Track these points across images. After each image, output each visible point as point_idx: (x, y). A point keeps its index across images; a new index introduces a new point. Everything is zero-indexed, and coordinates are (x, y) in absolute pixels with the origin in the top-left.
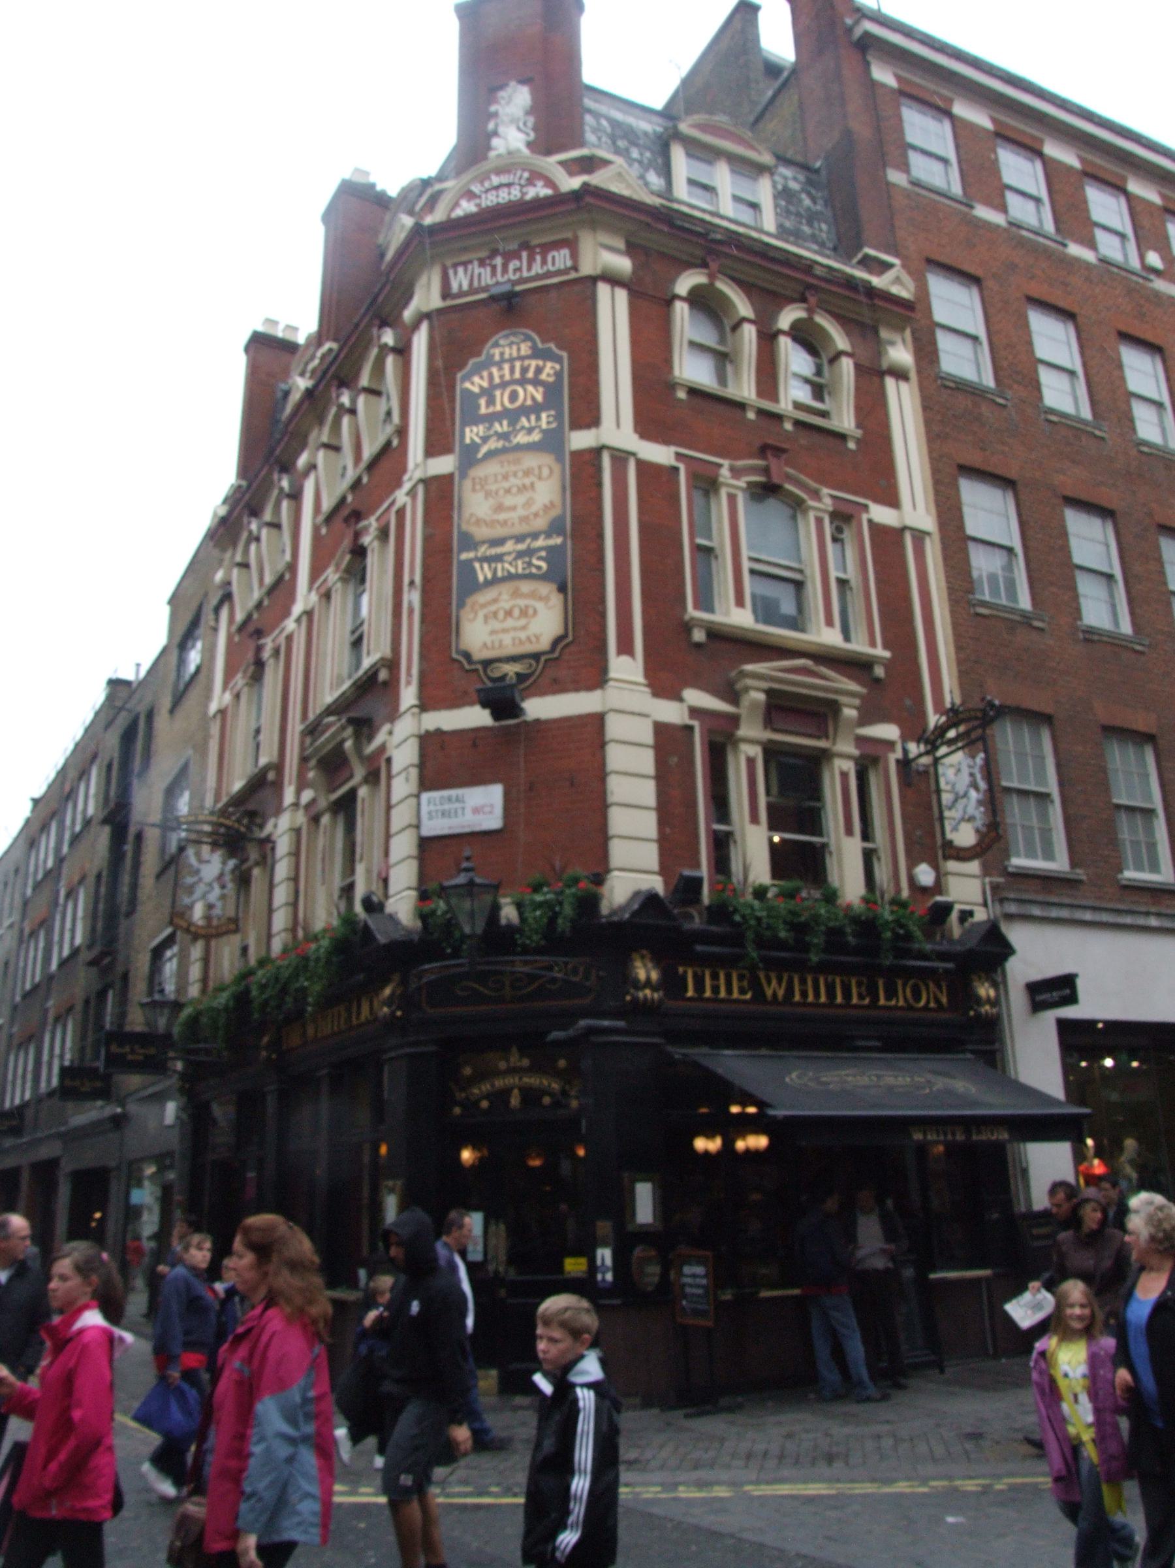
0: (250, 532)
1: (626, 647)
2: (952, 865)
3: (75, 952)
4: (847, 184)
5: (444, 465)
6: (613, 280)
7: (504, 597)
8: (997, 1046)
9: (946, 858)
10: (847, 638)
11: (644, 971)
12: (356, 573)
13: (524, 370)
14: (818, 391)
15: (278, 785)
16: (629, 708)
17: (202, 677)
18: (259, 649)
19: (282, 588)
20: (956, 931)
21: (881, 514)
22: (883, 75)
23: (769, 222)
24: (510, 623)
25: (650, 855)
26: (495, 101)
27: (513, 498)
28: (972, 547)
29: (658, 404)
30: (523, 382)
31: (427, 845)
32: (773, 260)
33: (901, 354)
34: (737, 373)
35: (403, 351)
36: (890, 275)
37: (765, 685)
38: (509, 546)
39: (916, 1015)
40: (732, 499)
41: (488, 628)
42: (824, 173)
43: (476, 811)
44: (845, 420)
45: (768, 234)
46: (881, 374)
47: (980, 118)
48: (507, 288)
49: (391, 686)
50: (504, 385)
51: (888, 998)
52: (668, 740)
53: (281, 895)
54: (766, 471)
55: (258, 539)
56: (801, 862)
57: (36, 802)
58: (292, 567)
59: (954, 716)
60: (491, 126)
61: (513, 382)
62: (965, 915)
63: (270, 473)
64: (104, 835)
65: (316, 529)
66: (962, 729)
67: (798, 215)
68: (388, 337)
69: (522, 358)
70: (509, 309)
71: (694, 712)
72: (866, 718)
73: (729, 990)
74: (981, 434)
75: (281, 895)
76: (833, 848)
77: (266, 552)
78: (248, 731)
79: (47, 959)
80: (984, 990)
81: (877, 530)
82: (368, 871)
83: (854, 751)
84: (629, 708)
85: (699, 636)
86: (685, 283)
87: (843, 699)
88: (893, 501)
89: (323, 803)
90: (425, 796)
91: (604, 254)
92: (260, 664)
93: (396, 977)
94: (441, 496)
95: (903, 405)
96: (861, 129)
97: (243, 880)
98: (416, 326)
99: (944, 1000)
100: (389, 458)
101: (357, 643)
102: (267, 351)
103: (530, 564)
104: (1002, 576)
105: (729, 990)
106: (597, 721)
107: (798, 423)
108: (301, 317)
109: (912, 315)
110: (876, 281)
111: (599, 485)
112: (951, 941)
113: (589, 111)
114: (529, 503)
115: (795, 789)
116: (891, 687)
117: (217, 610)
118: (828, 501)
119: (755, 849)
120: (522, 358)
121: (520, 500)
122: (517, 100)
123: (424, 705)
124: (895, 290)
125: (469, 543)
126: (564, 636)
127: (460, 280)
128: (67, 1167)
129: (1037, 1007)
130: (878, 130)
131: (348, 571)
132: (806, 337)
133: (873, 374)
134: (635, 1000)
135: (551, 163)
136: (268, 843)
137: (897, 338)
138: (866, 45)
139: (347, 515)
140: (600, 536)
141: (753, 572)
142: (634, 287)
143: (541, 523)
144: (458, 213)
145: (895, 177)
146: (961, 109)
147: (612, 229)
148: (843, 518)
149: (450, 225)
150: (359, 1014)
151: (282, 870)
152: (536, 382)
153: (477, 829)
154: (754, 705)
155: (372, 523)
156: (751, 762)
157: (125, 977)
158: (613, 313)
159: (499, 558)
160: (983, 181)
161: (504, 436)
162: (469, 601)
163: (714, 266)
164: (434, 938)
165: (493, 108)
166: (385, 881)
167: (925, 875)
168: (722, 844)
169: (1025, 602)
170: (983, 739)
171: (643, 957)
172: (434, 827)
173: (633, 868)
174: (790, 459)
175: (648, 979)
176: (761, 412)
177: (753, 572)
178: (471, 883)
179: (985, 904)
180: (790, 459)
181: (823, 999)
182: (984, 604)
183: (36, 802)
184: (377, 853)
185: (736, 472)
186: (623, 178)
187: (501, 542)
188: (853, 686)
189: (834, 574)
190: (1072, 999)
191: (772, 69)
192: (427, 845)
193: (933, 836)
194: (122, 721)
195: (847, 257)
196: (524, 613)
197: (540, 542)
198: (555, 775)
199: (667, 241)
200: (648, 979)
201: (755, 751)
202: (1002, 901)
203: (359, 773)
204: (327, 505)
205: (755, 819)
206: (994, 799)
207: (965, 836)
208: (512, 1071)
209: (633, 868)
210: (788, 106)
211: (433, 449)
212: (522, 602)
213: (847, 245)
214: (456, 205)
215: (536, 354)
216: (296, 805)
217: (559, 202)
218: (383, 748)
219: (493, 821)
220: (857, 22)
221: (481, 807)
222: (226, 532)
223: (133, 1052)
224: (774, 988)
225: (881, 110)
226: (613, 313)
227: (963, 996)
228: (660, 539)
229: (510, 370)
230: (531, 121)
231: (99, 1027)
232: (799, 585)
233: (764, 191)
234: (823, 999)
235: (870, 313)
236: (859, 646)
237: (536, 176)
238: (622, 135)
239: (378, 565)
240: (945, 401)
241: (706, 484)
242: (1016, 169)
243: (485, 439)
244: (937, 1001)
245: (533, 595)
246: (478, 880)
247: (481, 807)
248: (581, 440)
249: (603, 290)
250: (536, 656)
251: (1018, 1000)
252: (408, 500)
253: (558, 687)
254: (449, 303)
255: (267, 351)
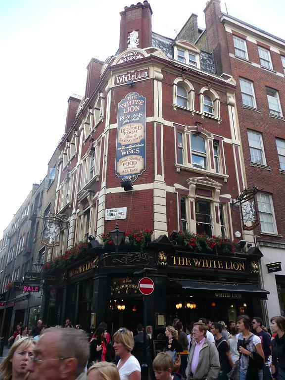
0: (68, 146)
1: (159, 172)
2: (246, 232)
3: (21, 252)
4: (218, 58)
5: (114, 126)
6: (158, 80)
7: (128, 159)
8: (258, 282)
9: (244, 230)
10: (217, 172)
11: (162, 257)
12: (92, 153)
13: (135, 102)
14: (211, 110)
15: (71, 208)
16: (160, 188)
17: (55, 181)
18: (68, 175)
19: (74, 159)
20: (247, 250)
21: (226, 140)
22: (229, 30)
23: (199, 66)
24: (130, 166)
25: (164, 226)
26: (130, 36)
27: (132, 133)
28: (242, 95)
29: (169, 112)
30: (134, 105)
31: (106, 222)
32: (199, 75)
33: (232, 99)
34: (190, 104)
35: (105, 98)
36: (230, 79)
37: (196, 183)
38: (130, 146)
39: (236, 272)
40: (188, 136)
41: (124, 167)
42: (213, 55)
43: (120, 214)
44: (217, 115)
45: (198, 69)
46: (227, 105)
47: (253, 40)
48: (131, 82)
49: (100, 182)
50: (130, 106)
51: (228, 267)
52: (170, 197)
53: (71, 236)
54: (197, 129)
55: (69, 147)
56: (204, 229)
57: (15, 215)
58: (77, 154)
59: (246, 192)
60: (128, 42)
61: (132, 105)
62: (249, 245)
63: (72, 131)
64: (29, 223)
65: (83, 144)
66: (248, 195)
67: (206, 65)
68: (101, 95)
69: (135, 99)
70: (132, 87)
71: (177, 189)
72: (222, 192)
73: (185, 262)
74: (252, 121)
75: (71, 236)
76: (213, 226)
77: (71, 150)
78: (65, 195)
79: (15, 254)
80: (255, 266)
81: (226, 144)
82: (92, 230)
83: (218, 200)
84: (160, 188)
85: (178, 170)
86: (176, 81)
87: (216, 187)
88: (230, 138)
89: (82, 213)
90: (106, 210)
91: (155, 72)
92: (68, 178)
93: (98, 257)
94: (113, 134)
95: (233, 113)
96: (223, 44)
97: (62, 233)
98: (108, 91)
99: (244, 268)
100: (101, 125)
101: (92, 172)
102: (73, 100)
103: (135, 151)
104: (258, 157)
105: (185, 262)
106: (152, 191)
107: (205, 117)
108: (80, 93)
109: (235, 90)
110: (227, 81)
111: (154, 131)
112: (245, 252)
113: (153, 38)
114: (135, 136)
115: (203, 209)
116: (229, 185)
117: (59, 165)
118: (213, 137)
119: (192, 227)
120: (135, 99)
121: (134, 135)
122: (134, 36)
123: (107, 187)
124: (231, 83)
125: (120, 145)
126: (144, 169)
127: (119, 80)
128: (15, 309)
129: (270, 271)
130: (227, 44)
131: (90, 154)
132: (207, 95)
133: (225, 105)
134: (160, 265)
135: (143, 51)
136: (68, 223)
137: (231, 96)
138: (224, 22)
139: (90, 140)
140: (154, 144)
141: (192, 154)
142: (163, 81)
143: (138, 141)
144: (119, 63)
145: (231, 55)
146: (249, 38)
147: (158, 67)
148: (216, 141)
149: (117, 66)
150: (88, 267)
151: (71, 230)
152: (138, 105)
153: (120, 219)
154: (192, 188)
155: (96, 142)
156: (192, 203)
157: (33, 259)
158: (158, 88)
159: (127, 149)
160: (254, 55)
161: (130, 119)
162: (119, 160)
163: (184, 77)
164: (109, 247)
165: (129, 37)
166: (96, 232)
167: (238, 234)
168: (184, 223)
169: (265, 164)
170: (254, 197)
171: (162, 253)
172: (108, 218)
173: (160, 229)
174: (202, 126)
175: (163, 259)
176: (195, 114)
177: (192, 154)
178: (117, 232)
179: (255, 243)
180: (202, 126)
181: (211, 266)
182: (254, 164)
183: (15, 215)
184: (95, 224)
185: (189, 129)
186: (160, 54)
187: (128, 145)
188: (219, 184)
189: (214, 155)
190: (280, 269)
191: (200, 31)
192: (106, 222)
193: (240, 224)
194: (36, 194)
195: (219, 75)
196: (133, 163)
197: (138, 146)
198: (142, 204)
199: (171, 69)
200: (163, 259)
201: (193, 200)
202: (259, 242)
203: (91, 204)
204: (86, 138)
205: (192, 218)
206: (257, 214)
207: (249, 224)
208: (126, 283)
209: (160, 229)
210: (204, 39)
211: (111, 123)
212: (133, 161)
213: (219, 72)
214: (119, 61)
215: (138, 98)
216: (75, 213)
217: (145, 59)
218: (97, 198)
219: (124, 217)
220: (222, 17)
221: (121, 213)
222: (62, 146)
223: (31, 278)
224: (197, 263)
225: (228, 38)
226: (158, 88)
227: (249, 267)
228: (169, 145)
229: (132, 100)
230: (138, 40)
231: (25, 270)
232: (205, 158)
233: (197, 59)
234: (211, 266)
235: (224, 88)
236: (221, 173)
237: (138, 53)
238: (161, 44)
239: (98, 152)
240: (244, 113)
241: (181, 131)
242: (263, 54)
243: (125, 120)
244: (242, 268)
245: (135, 159)
246: (119, 231)
247: (121, 213)
248: (149, 119)
249: (155, 82)
250: (136, 174)
251: (264, 269)
252: (105, 135)
253: (141, 182)
254: (116, 86)
255: (73, 100)
